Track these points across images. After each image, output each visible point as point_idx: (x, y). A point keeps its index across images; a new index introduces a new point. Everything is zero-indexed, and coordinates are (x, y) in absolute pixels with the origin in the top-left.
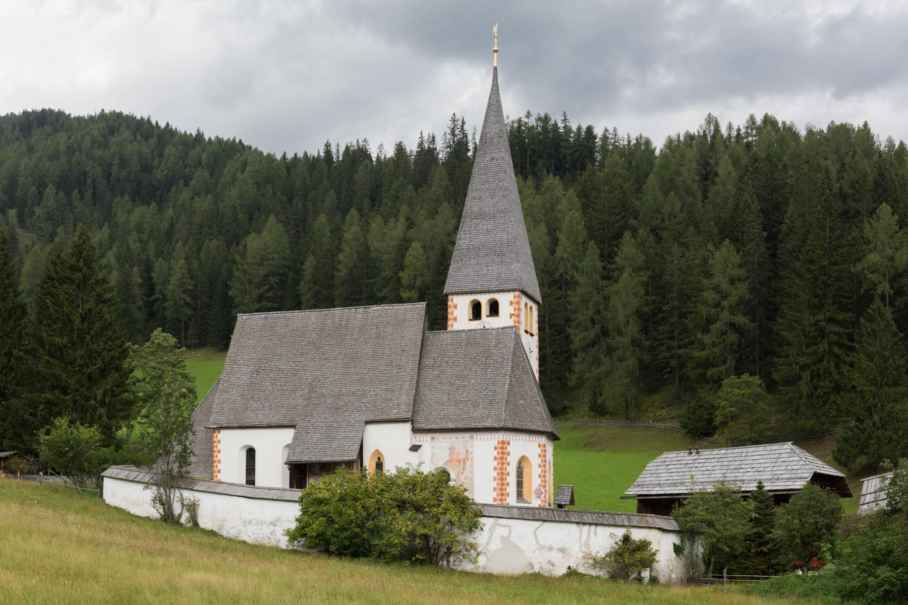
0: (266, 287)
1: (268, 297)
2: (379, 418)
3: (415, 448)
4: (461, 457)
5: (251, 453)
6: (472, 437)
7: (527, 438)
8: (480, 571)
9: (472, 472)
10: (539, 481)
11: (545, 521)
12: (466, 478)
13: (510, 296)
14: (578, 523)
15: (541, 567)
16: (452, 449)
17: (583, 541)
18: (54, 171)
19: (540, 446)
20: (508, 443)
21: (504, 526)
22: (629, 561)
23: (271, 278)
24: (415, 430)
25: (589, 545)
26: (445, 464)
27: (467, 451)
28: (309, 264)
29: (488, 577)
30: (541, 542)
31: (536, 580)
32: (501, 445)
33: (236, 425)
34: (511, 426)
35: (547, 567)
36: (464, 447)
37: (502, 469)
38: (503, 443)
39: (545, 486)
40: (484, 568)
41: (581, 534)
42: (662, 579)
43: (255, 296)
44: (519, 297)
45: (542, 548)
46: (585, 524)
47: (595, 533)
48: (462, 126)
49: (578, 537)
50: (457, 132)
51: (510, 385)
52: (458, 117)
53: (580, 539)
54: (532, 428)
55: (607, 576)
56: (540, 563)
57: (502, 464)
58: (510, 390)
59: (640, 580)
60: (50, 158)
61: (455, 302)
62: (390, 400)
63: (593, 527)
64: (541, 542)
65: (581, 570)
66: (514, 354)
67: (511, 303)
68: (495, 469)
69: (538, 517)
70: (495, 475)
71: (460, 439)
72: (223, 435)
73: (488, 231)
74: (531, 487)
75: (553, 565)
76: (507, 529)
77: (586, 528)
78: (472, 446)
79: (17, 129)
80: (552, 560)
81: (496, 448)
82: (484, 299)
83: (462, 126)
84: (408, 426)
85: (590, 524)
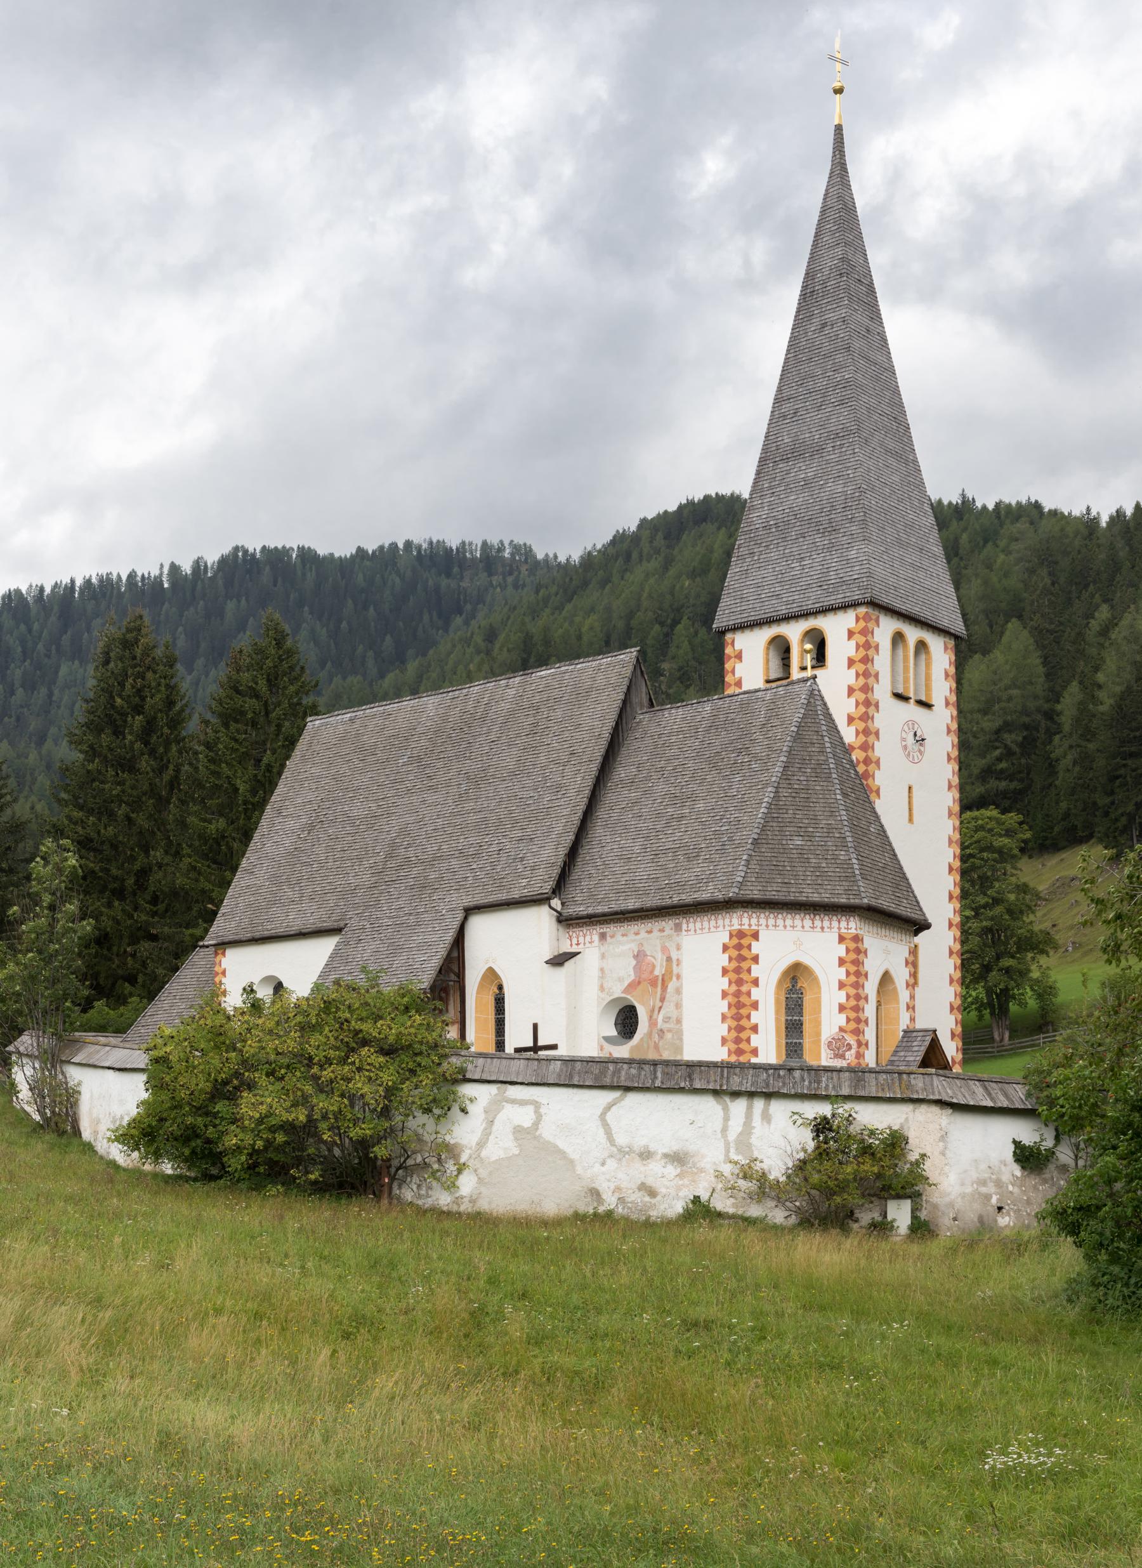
0: (997, 752)
1: (1002, 771)
2: (492, 899)
3: (559, 961)
4: (657, 972)
6: (678, 928)
7: (808, 922)
8: (465, 1207)
9: (678, 1006)
10: (841, 1020)
11: (628, 1089)
12: (667, 1019)
13: (847, 620)
14: (716, 1093)
15: (621, 1200)
16: (639, 956)
17: (732, 1136)
18: (698, 596)
19: (842, 939)
20: (756, 936)
21: (523, 1103)
22: (851, 1183)
23: (1006, 736)
24: (565, 921)
25: (749, 1146)
26: (625, 991)
27: (669, 959)
30: (621, 1140)
32: (735, 941)
35: (638, 1198)
36: (664, 949)
38: (741, 934)
39: (857, 1032)
40: (473, 1201)
41: (726, 1119)
42: (946, 1226)
43: (976, 771)
44: (867, 618)
45: (623, 1153)
46: (736, 1094)
47: (766, 1117)
49: (718, 1125)
51: (775, 805)
53: (724, 1130)
54: (815, 898)
55: (793, 1220)
56: (618, 1189)
57: (740, 982)
58: (768, 818)
59: (882, 1227)
61: (737, 646)
62: (522, 859)
63: (759, 1104)
64: (621, 1140)
65: (723, 1204)
66: (797, 737)
67: (851, 634)
68: (724, 994)
69: (607, 1081)
70: (725, 1009)
71: (656, 934)
73: (807, 483)
74: (818, 1034)
75: (652, 1193)
76: (530, 1109)
77: (739, 1107)
78: (678, 948)
79: (660, 535)
80: (650, 1181)
81: (725, 948)
85: (751, 1095)
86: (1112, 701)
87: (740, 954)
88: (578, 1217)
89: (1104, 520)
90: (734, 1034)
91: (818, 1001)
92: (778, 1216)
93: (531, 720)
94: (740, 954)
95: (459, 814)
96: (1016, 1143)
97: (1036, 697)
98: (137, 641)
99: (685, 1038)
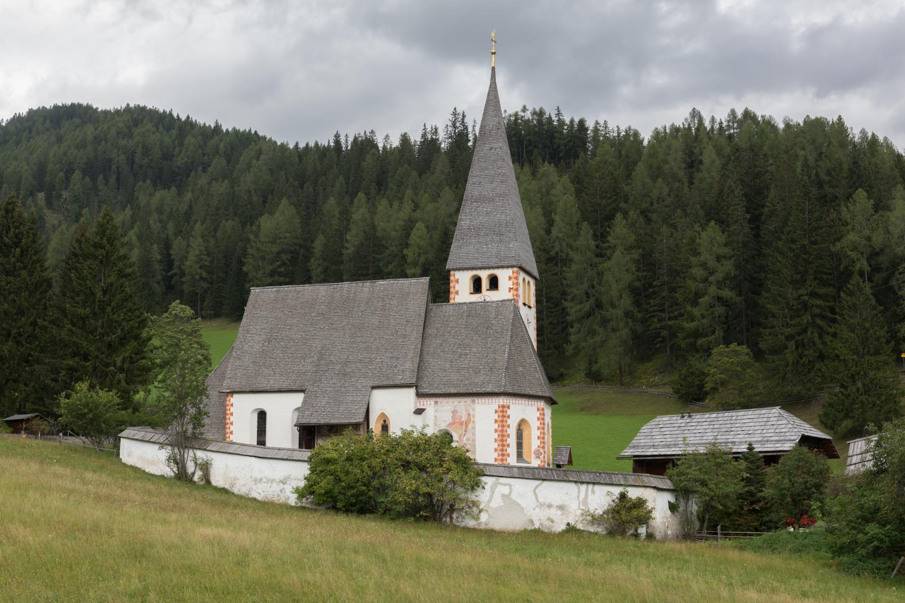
1: (280, 272)
2: (385, 383)
5: (262, 416)
6: (473, 402)
8: (483, 527)
9: (474, 434)
10: (538, 442)
12: (468, 439)
13: (509, 272)
14: (576, 482)
19: (538, 409)
20: (509, 407)
21: (505, 485)
24: (419, 395)
25: (587, 503)
27: (469, 414)
28: (319, 244)
29: (490, 533)
30: (541, 500)
31: (535, 538)
33: (248, 389)
34: (511, 391)
35: (547, 523)
36: (466, 410)
37: (502, 431)
38: (503, 406)
39: (543, 447)
42: (658, 535)
44: (517, 273)
45: (541, 505)
46: (582, 483)
47: (593, 492)
48: (463, 119)
49: (576, 495)
50: (458, 125)
51: (510, 353)
52: (458, 111)
53: (578, 496)
54: (531, 393)
57: (503, 426)
59: (636, 536)
60: (78, 147)
61: (456, 277)
62: (396, 367)
63: (591, 486)
64: (541, 500)
65: (580, 526)
66: (513, 325)
67: (510, 278)
68: (496, 431)
69: (537, 477)
72: (236, 399)
73: (487, 213)
75: (553, 522)
77: (583, 487)
79: (48, 121)
80: (551, 517)
82: (484, 275)
83: (463, 119)
84: (412, 391)
85: (588, 483)
86: (353, 249)
87: (503, 412)
88: (525, 531)
89: (279, 144)
90: (501, 447)
91: (530, 435)
92: (600, 530)
93: (380, 304)
94: (503, 412)
95: (352, 343)
96: (669, 503)
97: (297, 238)
98: (14, 209)
99: (477, 447)
